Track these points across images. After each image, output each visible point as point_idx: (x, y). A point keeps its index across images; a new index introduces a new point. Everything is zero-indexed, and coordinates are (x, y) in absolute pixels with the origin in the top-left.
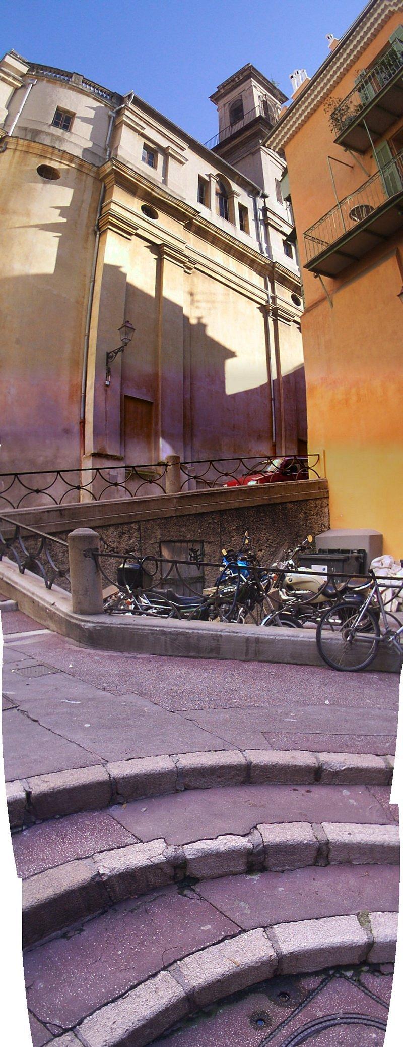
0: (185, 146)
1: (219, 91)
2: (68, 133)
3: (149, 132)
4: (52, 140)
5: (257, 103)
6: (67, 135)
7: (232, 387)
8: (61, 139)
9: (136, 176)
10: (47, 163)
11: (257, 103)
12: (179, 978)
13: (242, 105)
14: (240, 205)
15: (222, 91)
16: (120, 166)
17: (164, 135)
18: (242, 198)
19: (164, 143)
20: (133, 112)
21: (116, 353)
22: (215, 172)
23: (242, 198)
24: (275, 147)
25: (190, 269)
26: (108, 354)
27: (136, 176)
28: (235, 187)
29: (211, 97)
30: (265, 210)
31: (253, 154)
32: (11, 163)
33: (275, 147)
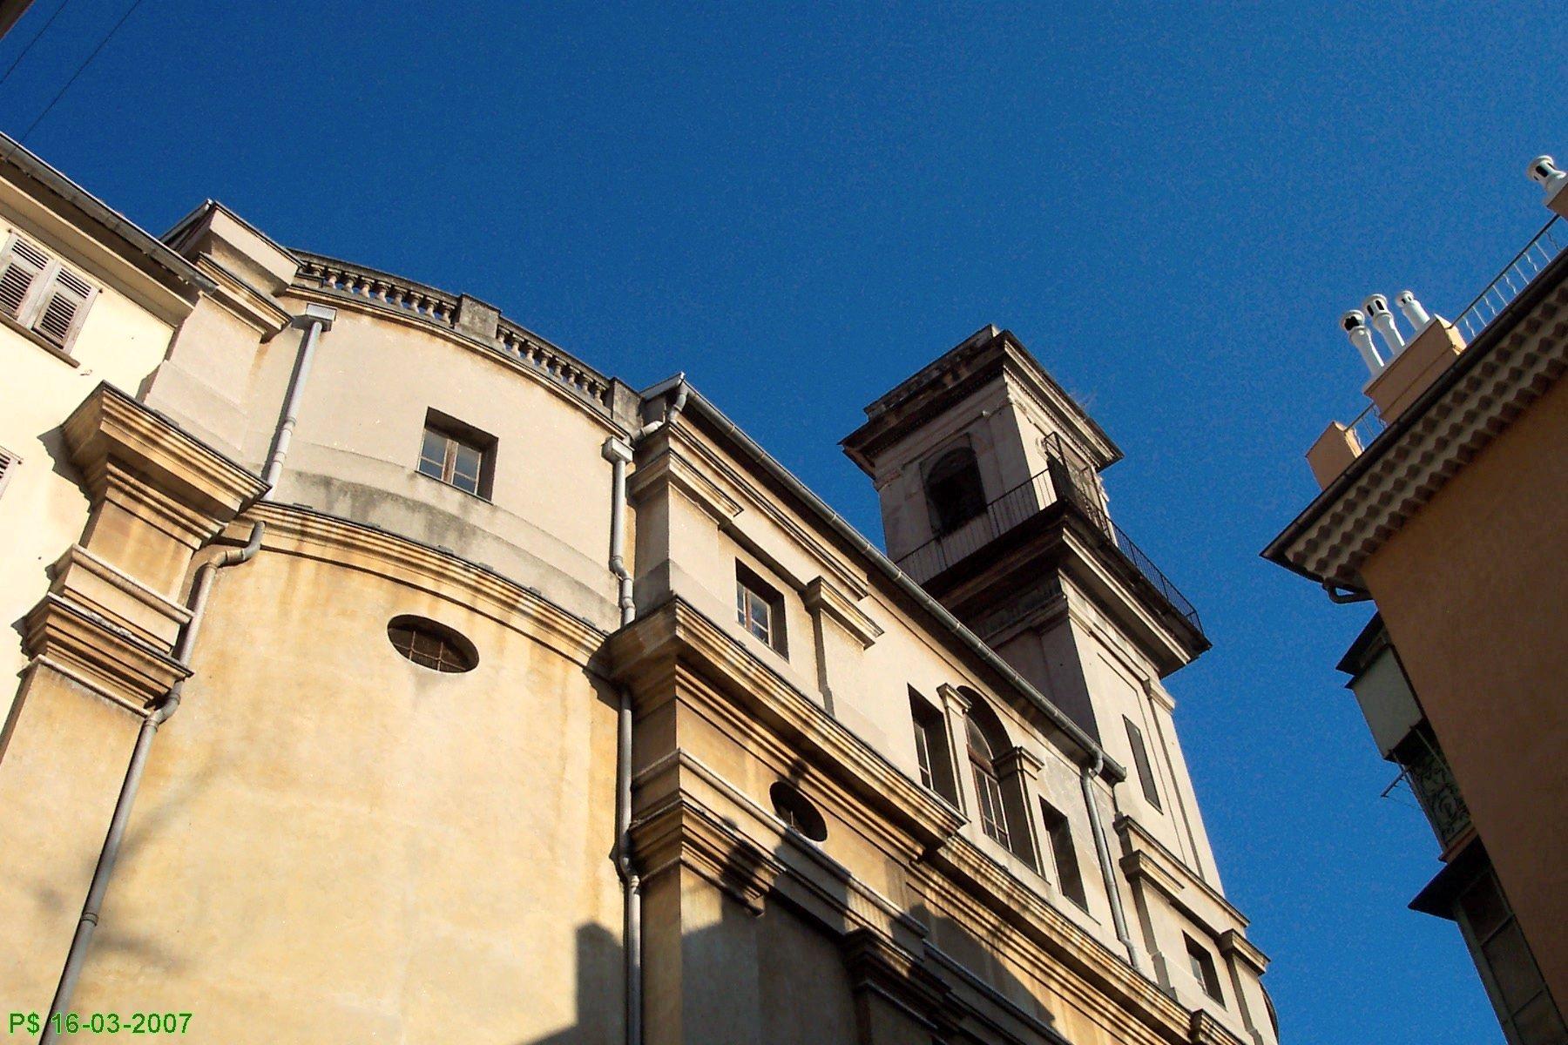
0: (860, 577)
1: (876, 422)
2: (482, 507)
3: (751, 523)
4: (430, 527)
5: (1037, 463)
6: (478, 514)
7: (683, 931)
8: (464, 530)
10: (422, 607)
11: (1037, 463)
12: (432, 609)
13: (972, 471)
14: (1044, 804)
15: (893, 422)
18: (1050, 778)
19: (805, 571)
23: (1050, 778)
28: (1018, 734)
29: (850, 442)
30: (1124, 825)
31: (1038, 631)
32: (285, 602)
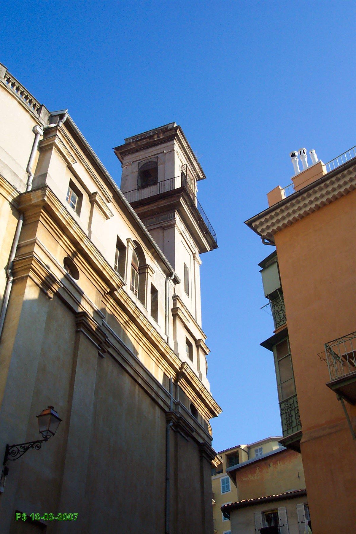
0: (110, 195)
1: (128, 144)
3: (78, 168)
5: (178, 173)
9: (67, 218)
11: (178, 173)
13: (156, 170)
15: (133, 146)
16: (53, 200)
17: (92, 177)
18: (156, 277)
19: (93, 188)
20: (64, 136)
21: (26, 450)
22: (133, 236)
23: (156, 277)
24: (263, 231)
25: (104, 351)
26: (8, 446)
27: (67, 218)
29: (117, 149)
30: (176, 298)
31: (164, 228)
33: (263, 231)
